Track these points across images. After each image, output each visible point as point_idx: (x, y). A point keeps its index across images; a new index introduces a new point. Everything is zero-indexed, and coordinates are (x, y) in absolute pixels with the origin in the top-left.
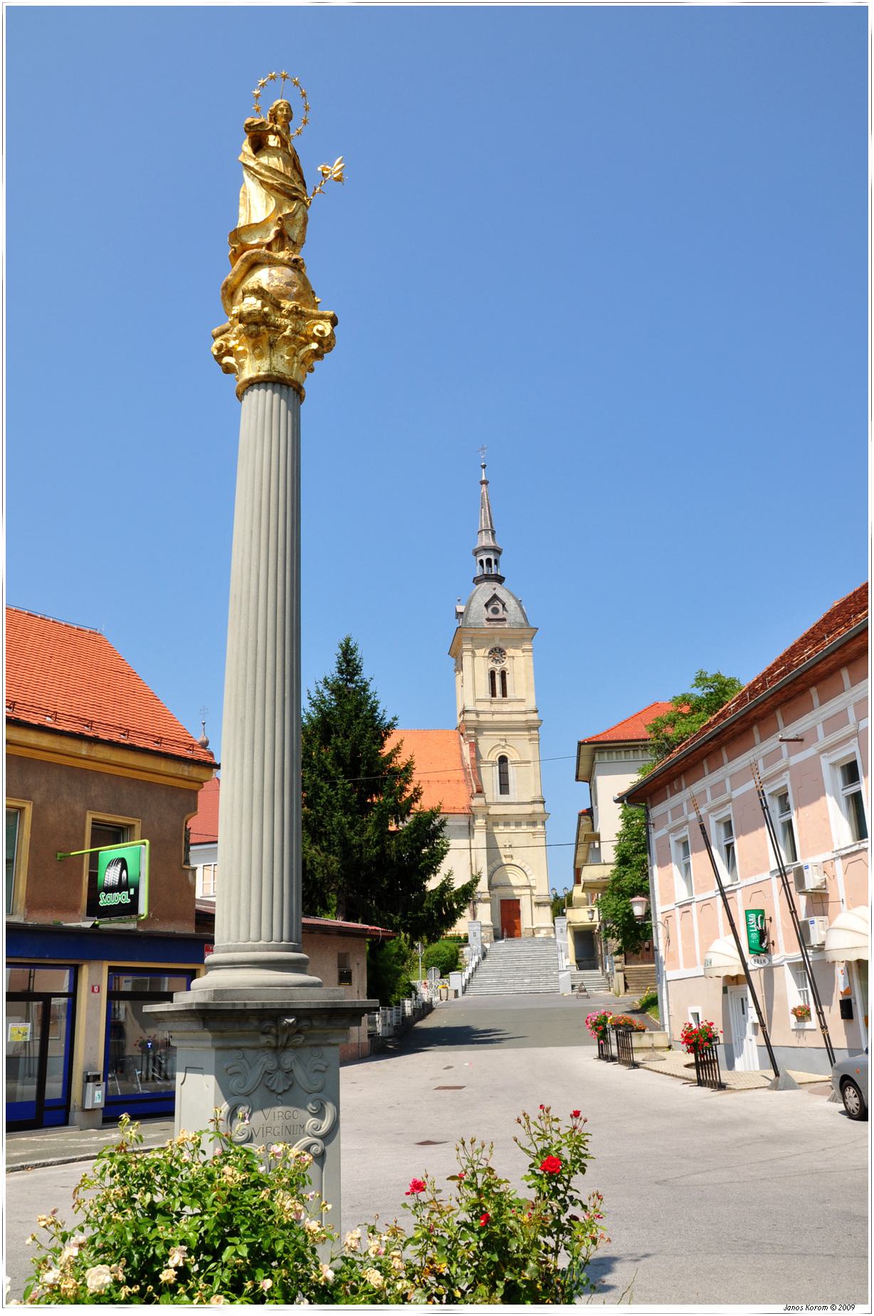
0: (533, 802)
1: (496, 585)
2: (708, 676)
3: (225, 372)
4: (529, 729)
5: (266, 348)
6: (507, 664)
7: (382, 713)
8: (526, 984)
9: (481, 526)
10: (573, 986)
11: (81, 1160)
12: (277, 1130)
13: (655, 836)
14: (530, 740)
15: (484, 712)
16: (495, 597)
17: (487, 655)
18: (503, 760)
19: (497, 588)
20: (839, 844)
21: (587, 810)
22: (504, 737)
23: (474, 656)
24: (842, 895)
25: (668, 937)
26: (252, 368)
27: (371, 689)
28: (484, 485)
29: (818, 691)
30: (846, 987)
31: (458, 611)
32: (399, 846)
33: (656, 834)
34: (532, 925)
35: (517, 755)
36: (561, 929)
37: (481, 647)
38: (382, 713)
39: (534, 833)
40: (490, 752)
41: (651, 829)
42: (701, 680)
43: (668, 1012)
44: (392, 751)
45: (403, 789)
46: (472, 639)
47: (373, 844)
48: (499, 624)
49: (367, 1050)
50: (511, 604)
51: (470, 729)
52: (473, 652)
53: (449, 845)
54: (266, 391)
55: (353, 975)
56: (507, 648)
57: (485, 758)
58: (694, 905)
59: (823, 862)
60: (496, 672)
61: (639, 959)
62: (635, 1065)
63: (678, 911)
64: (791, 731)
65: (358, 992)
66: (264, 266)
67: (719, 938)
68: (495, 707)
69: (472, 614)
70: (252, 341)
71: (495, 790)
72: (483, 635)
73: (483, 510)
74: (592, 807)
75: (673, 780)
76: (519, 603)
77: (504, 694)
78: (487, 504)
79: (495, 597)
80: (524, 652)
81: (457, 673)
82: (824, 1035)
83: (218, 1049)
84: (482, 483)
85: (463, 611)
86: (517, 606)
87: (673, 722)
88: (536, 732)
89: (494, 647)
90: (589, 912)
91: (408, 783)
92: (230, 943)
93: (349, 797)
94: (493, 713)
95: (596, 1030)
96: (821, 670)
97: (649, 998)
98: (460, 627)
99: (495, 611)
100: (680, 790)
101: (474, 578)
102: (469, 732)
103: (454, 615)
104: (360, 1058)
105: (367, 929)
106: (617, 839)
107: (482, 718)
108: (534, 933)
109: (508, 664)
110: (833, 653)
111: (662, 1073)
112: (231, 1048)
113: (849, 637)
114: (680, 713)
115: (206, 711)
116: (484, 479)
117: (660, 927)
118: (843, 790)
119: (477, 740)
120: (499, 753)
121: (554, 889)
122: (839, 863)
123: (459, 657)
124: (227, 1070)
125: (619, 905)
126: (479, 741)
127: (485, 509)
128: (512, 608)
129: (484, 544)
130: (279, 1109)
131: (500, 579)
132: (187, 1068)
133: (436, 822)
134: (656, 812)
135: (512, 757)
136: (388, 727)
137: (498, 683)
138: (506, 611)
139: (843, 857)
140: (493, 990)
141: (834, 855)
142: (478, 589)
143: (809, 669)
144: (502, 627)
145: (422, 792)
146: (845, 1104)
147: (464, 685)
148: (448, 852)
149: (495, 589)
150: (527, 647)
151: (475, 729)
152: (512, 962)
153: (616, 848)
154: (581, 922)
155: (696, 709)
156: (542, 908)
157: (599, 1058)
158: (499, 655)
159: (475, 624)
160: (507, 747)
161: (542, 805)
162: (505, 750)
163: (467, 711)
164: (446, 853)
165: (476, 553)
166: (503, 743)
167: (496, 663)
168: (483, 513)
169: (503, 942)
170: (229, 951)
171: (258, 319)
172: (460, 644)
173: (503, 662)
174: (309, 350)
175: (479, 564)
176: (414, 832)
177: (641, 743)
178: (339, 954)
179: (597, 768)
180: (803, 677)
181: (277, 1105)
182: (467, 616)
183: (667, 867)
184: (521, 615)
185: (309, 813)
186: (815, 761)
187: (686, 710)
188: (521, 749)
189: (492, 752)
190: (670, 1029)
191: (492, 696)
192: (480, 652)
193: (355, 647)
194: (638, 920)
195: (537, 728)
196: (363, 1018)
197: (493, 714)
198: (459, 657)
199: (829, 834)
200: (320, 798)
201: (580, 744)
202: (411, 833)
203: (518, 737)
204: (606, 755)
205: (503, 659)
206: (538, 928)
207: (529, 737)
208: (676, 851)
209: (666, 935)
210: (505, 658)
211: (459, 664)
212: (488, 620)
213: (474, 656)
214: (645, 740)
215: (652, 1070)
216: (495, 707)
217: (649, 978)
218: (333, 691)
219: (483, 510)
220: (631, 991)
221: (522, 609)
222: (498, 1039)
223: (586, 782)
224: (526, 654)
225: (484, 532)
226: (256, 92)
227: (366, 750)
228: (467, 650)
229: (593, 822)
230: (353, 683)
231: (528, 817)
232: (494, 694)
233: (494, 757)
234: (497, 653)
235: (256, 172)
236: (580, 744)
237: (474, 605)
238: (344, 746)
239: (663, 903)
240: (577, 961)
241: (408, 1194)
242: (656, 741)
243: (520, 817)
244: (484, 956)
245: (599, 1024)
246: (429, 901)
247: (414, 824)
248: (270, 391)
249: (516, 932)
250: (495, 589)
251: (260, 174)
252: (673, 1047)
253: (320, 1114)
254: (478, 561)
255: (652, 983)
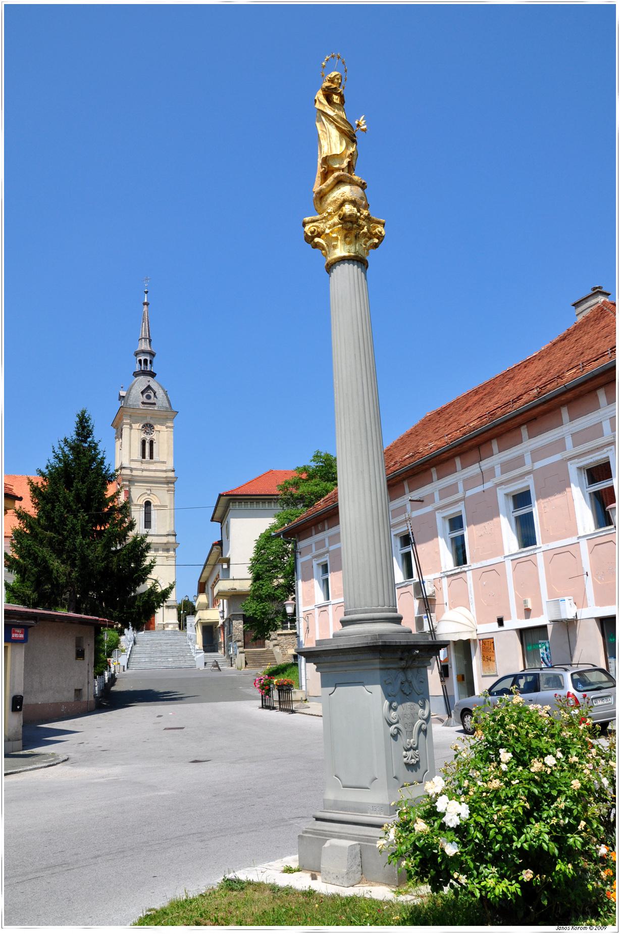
0: (168, 535)
1: (149, 378)
2: (322, 454)
3: (313, 247)
4: (168, 483)
5: (353, 239)
6: (154, 436)
7: (107, 466)
8: (170, 662)
9: (142, 335)
10: (205, 663)
11: (31, 770)
12: (408, 716)
13: (301, 560)
14: (168, 491)
15: (136, 469)
16: (149, 387)
17: (141, 428)
18: (148, 504)
19: (151, 381)
20: (445, 567)
21: (218, 541)
22: (149, 488)
23: (131, 428)
24: (446, 600)
25: (308, 628)
26: (341, 251)
27: (100, 447)
28: (145, 306)
29: (437, 470)
30: (445, 657)
31: (121, 395)
32: (119, 561)
33: (301, 559)
34: (163, 621)
35: (158, 501)
36: (191, 624)
37: (136, 422)
38: (107, 466)
39: (167, 557)
40: (138, 499)
41: (298, 555)
42: (317, 456)
43: (306, 677)
44: (115, 493)
45: (123, 521)
46: (130, 416)
47: (101, 559)
48: (151, 407)
49: (93, 706)
50: (160, 393)
51: (126, 480)
52: (131, 426)
53: (155, 562)
54: (354, 266)
55: (85, 652)
56: (155, 425)
57: (135, 502)
58: (330, 607)
59: (434, 579)
60: (147, 441)
61: (253, 645)
62: (293, 712)
63: (317, 611)
64: (416, 494)
65: (88, 665)
66: (346, 184)
67: (543, 614)
68: (145, 466)
69: (132, 398)
70: (345, 232)
71: (141, 525)
72: (139, 413)
73: (144, 324)
74: (222, 540)
75: (319, 523)
76: (166, 393)
77: (151, 457)
78: (147, 320)
79: (149, 387)
80: (167, 428)
81: (117, 440)
82: (442, 686)
83: (381, 669)
84: (145, 304)
85: (124, 395)
86: (164, 395)
87: (296, 485)
88: (172, 485)
89: (146, 423)
90: (220, 612)
91: (126, 517)
92: (366, 608)
93: (87, 526)
94: (143, 470)
95: (263, 689)
96: (443, 457)
97: (271, 670)
98: (122, 407)
99: (149, 397)
100: (324, 530)
101: (134, 372)
102: (124, 483)
103: (118, 398)
104: (89, 712)
105: (98, 620)
106: (250, 562)
107: (135, 473)
108: (164, 628)
109: (155, 436)
110: (455, 447)
111: (315, 715)
112: (389, 669)
113: (469, 438)
114: (301, 478)
116: (146, 301)
117: (302, 620)
118: (449, 534)
119: (130, 489)
120: (148, 498)
121: (187, 596)
122: (445, 580)
123: (120, 428)
124: (385, 681)
125: (258, 607)
126: (131, 490)
127: (145, 323)
128: (161, 396)
129: (143, 349)
130: (408, 704)
131: (153, 375)
132: (336, 684)
133: (144, 546)
134: (302, 544)
135: (155, 501)
136: (111, 476)
137: (147, 449)
138: (156, 398)
139: (448, 576)
140: (149, 666)
141: (442, 575)
142: (137, 380)
143: (436, 456)
144: (152, 409)
145: (136, 524)
146: (464, 726)
147: (123, 449)
148: (154, 567)
149: (149, 381)
150: (170, 425)
151: (129, 481)
152: (156, 647)
153: (250, 569)
154: (208, 620)
155: (311, 477)
156: (170, 610)
157: (262, 707)
158: (149, 429)
159: (134, 405)
160: (151, 495)
161: (174, 537)
162: (149, 497)
163: (124, 468)
164: (152, 568)
165: (137, 354)
166: (149, 492)
167: (147, 435)
168: (144, 325)
169: (143, 632)
170: (366, 613)
171: (354, 220)
172: (121, 419)
173: (152, 434)
174: (373, 243)
175: (138, 362)
176: (131, 552)
177: (275, 497)
178: (76, 637)
179: (231, 513)
180: (431, 461)
181: (408, 702)
182: (128, 399)
183: (309, 581)
184: (167, 402)
185: (52, 536)
186: (432, 515)
187: (304, 476)
188: (161, 497)
189: (140, 498)
190: (306, 688)
191: (143, 458)
192: (136, 426)
193: (88, 417)
194: (289, 616)
195: (173, 483)
196: (440, 651)
197: (142, 471)
198: (120, 428)
199: (439, 561)
200: (67, 525)
201: (220, 496)
202: (129, 553)
203: (157, 488)
204: (237, 504)
205: (152, 432)
206: (167, 624)
207: (167, 489)
208: (317, 571)
209: (306, 627)
210: (153, 431)
211: (119, 433)
212: (143, 403)
213: (131, 428)
214: (278, 495)
215: (306, 714)
216: (145, 466)
217: (261, 657)
218: (72, 448)
219: (144, 324)
220: (249, 666)
221: (167, 397)
222: (179, 698)
223: (219, 522)
224: (169, 429)
225: (143, 340)
226: (324, 64)
227: (98, 493)
228: (127, 424)
229: (222, 550)
230: (86, 443)
231: (163, 545)
232: (144, 457)
233: (142, 502)
234: (148, 427)
235: (334, 120)
236: (220, 496)
237: (133, 391)
238: (82, 489)
239: (305, 604)
240: (203, 646)
242: (283, 497)
243: (158, 545)
244: (135, 643)
245: (265, 685)
246: (140, 601)
247: (132, 546)
248: (356, 266)
249: (152, 626)
250: (149, 381)
251: (337, 122)
252: (308, 700)
253: (423, 707)
254: (138, 360)
255: (263, 661)
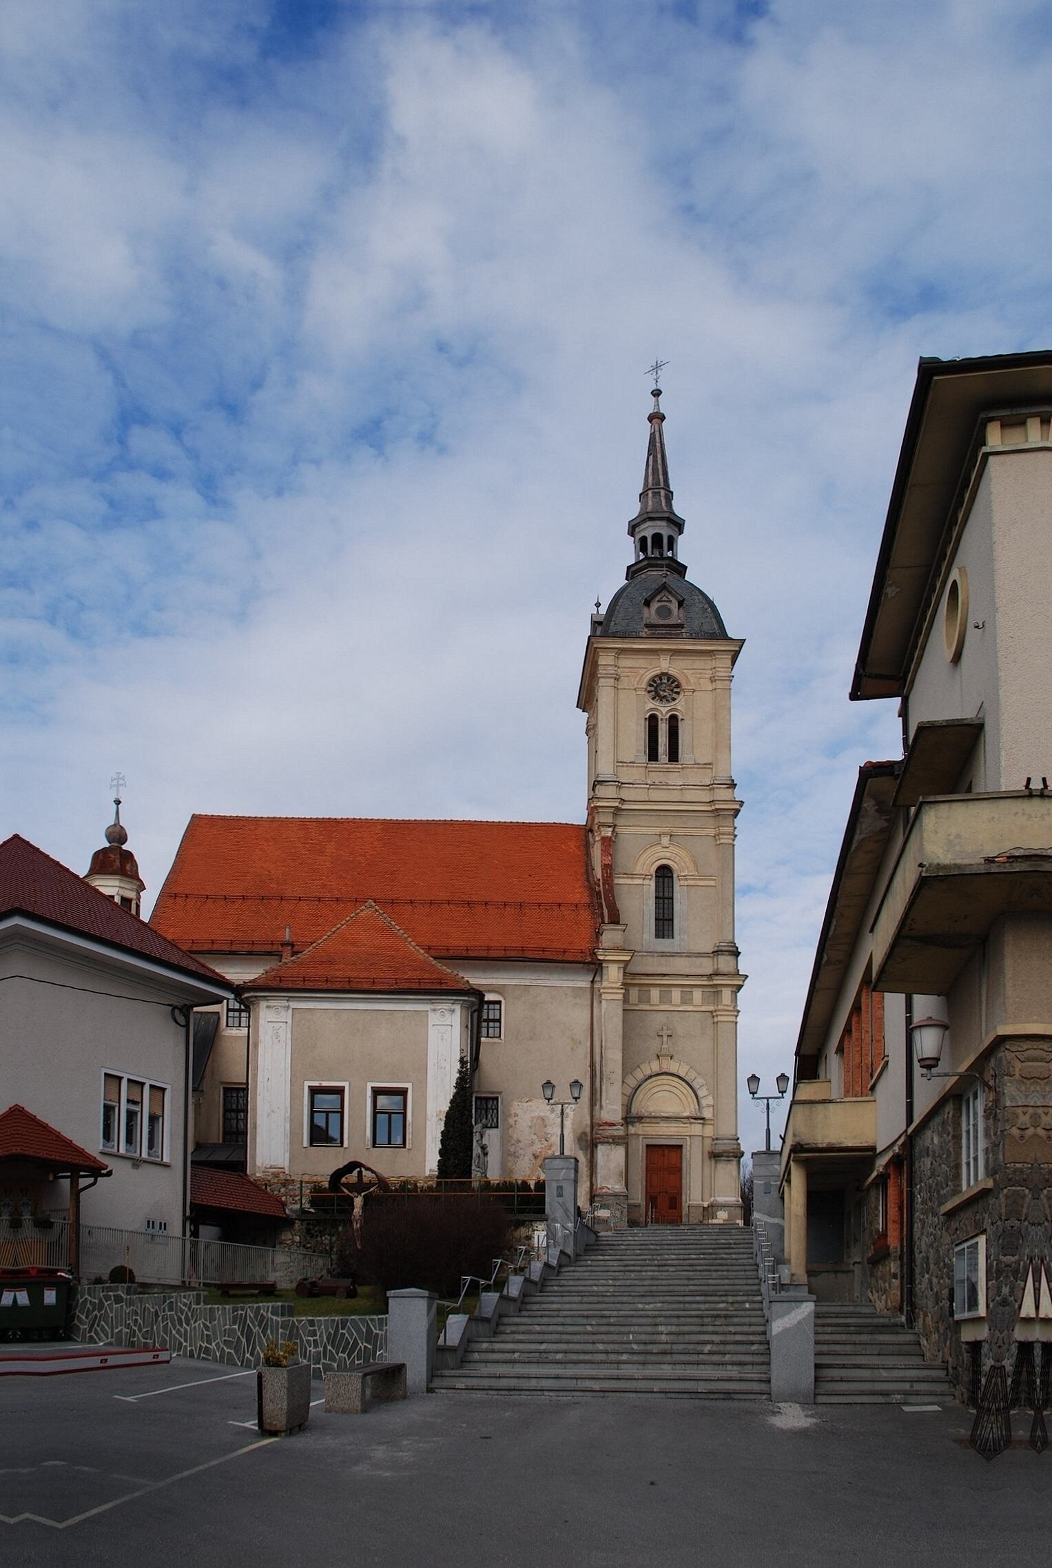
68: (656, 777)
77: (674, 756)
115: (121, 782)
173: (674, 699)
241: (836, 1278)
